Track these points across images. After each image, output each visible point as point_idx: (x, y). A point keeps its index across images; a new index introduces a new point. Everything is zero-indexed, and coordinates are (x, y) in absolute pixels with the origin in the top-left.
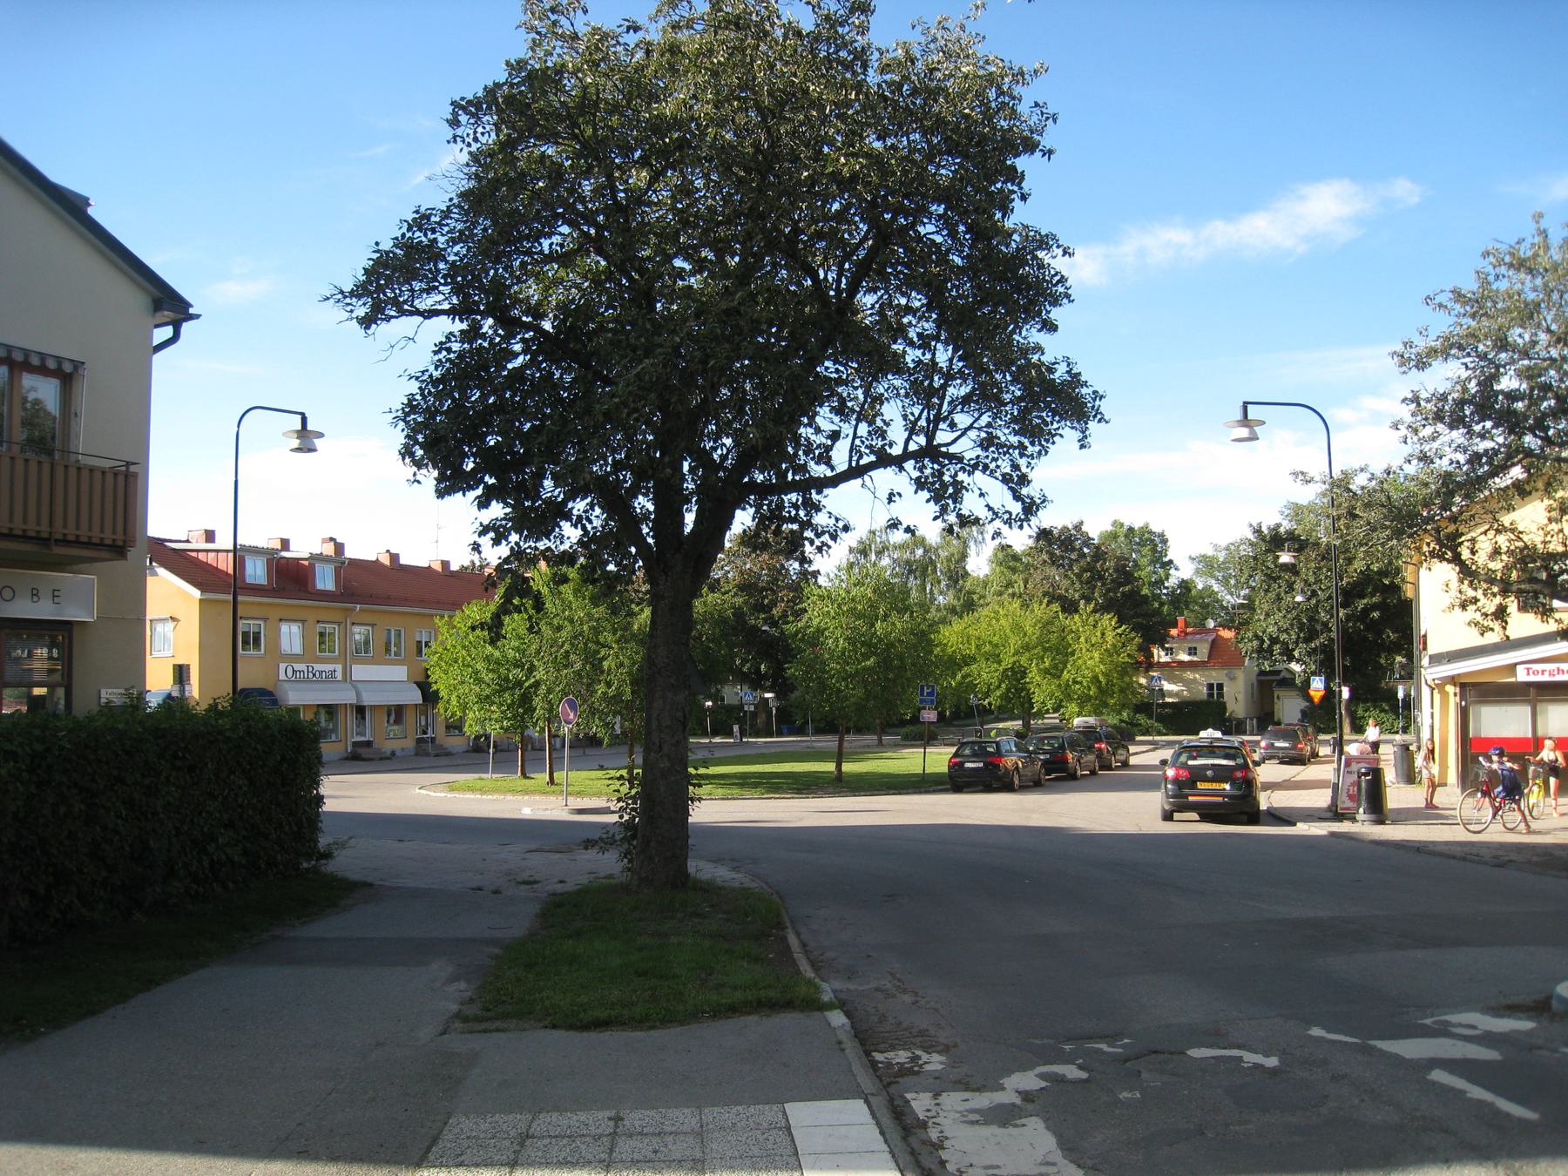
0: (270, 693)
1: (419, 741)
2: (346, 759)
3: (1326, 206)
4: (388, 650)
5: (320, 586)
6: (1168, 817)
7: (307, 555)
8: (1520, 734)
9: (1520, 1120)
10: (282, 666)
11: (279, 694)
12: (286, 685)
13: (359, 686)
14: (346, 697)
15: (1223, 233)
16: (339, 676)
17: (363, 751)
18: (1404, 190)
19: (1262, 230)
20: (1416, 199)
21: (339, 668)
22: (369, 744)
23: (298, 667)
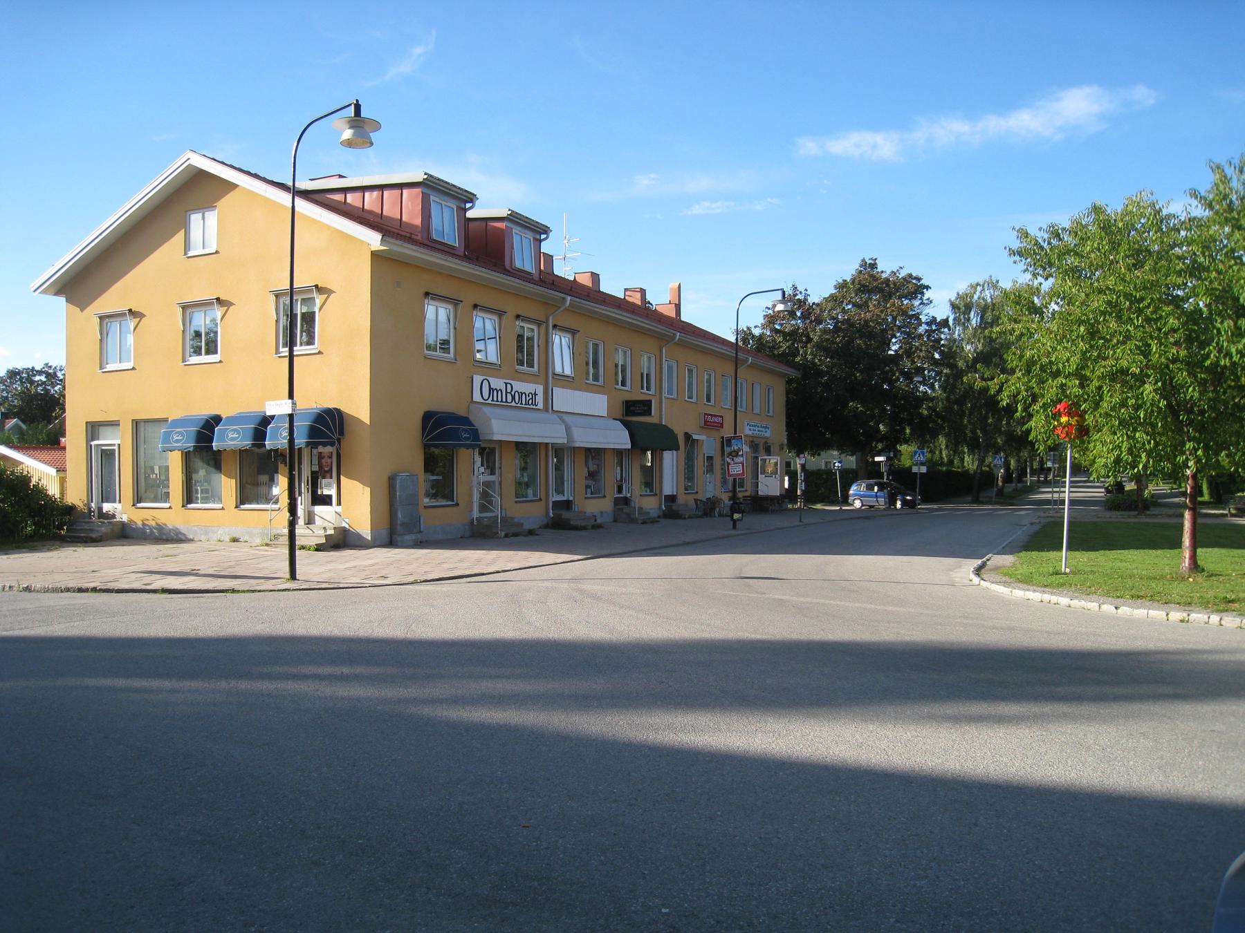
0: (465, 421)
1: (617, 501)
2: (547, 526)
3: (1078, 105)
4: (708, 399)
5: (518, 264)
6: (677, 449)
7: (504, 213)
8: (1204, 550)
9: (1226, 869)
10: (478, 379)
11: (477, 422)
12: (487, 410)
13: (567, 418)
14: (552, 434)
15: (993, 124)
16: (540, 399)
17: (565, 515)
18: (1143, 95)
19: (1026, 122)
20: (1152, 102)
21: (540, 389)
22: (567, 505)
23: (498, 383)
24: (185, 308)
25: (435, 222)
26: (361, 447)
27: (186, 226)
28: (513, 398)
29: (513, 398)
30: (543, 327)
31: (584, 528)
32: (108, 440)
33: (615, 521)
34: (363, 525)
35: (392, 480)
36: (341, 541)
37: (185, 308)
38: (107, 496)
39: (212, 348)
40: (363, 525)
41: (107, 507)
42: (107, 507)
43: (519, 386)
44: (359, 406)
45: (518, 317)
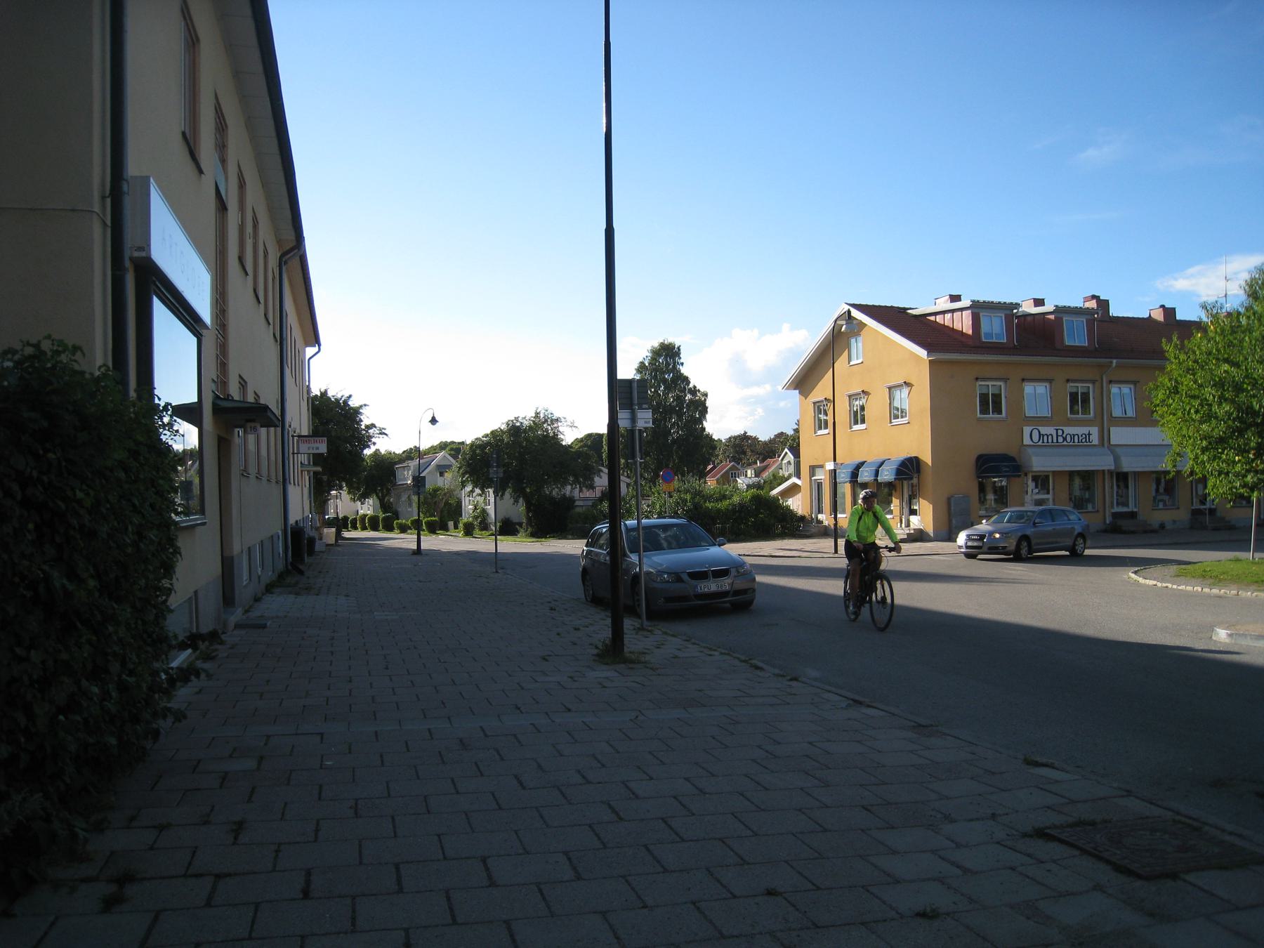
2: (1105, 531)
10: (1027, 430)
12: (1030, 451)
13: (1118, 450)
14: (1104, 462)
21: (1094, 431)
23: (1044, 430)
24: (890, 388)
25: (985, 327)
26: (928, 478)
27: (849, 347)
28: (1065, 439)
29: (1065, 439)
30: (1097, 384)
31: (1133, 532)
32: (820, 476)
33: (1192, 528)
34: (930, 530)
35: (949, 499)
36: (919, 536)
37: (890, 388)
38: (820, 511)
39: (984, 398)
40: (930, 530)
41: (820, 516)
42: (820, 516)
43: (1069, 430)
44: (927, 457)
45: (1068, 381)
